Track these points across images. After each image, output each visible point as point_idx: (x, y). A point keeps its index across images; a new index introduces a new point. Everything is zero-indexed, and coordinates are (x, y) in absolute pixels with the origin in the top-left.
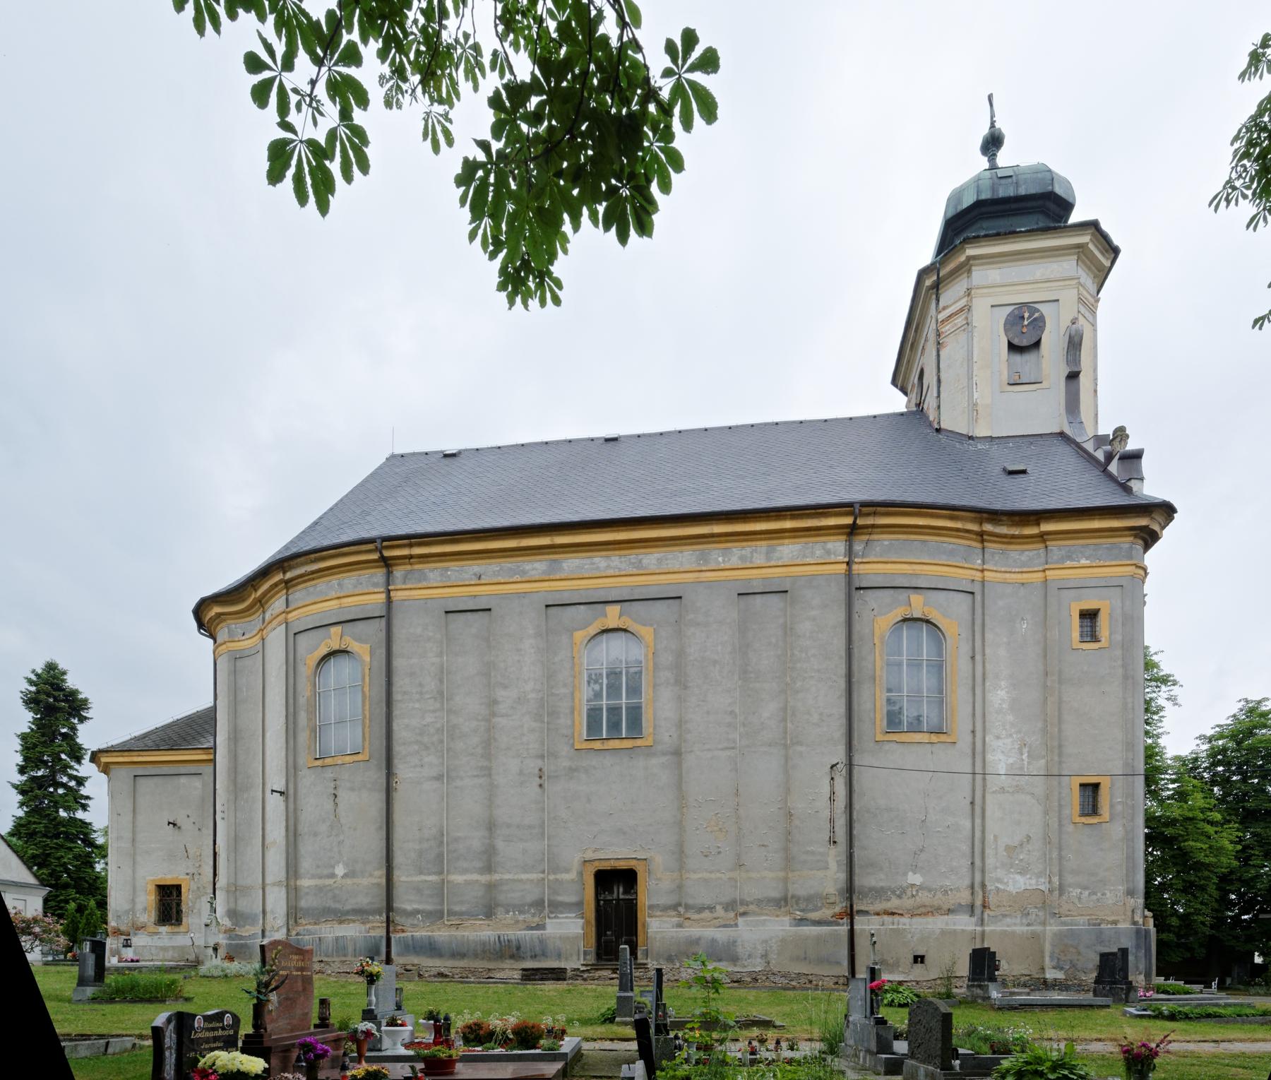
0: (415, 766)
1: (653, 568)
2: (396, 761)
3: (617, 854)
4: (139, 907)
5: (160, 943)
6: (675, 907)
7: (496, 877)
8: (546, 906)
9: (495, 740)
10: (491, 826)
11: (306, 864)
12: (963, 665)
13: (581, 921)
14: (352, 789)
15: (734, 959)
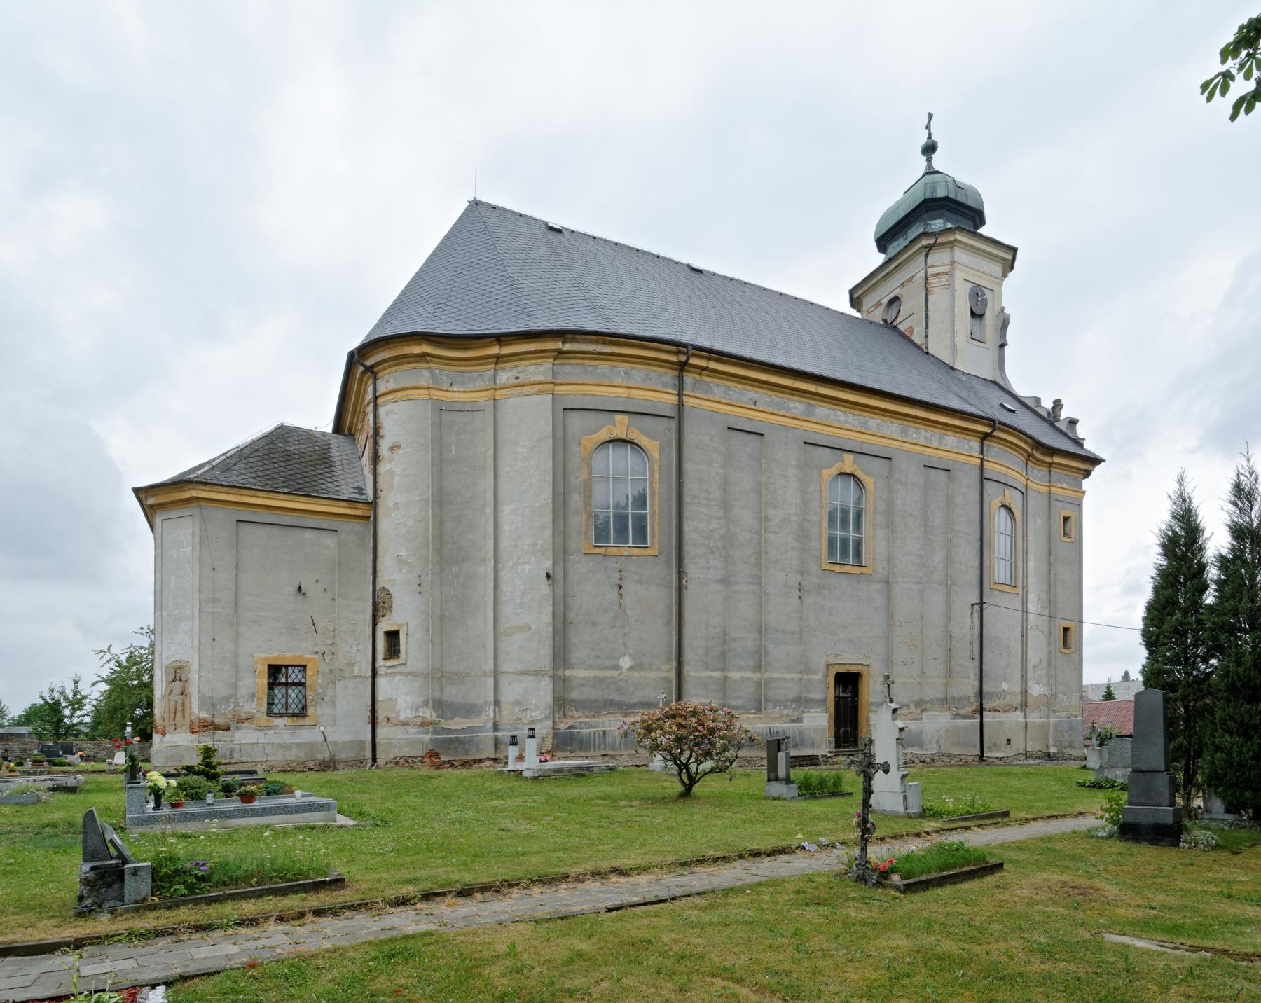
0: (703, 568)
1: (874, 431)
3: (849, 660)
4: (243, 692)
5: (276, 740)
7: (767, 675)
8: (802, 702)
9: (767, 553)
10: (761, 630)
11: (579, 653)
13: (827, 715)
14: (640, 582)
15: (921, 745)
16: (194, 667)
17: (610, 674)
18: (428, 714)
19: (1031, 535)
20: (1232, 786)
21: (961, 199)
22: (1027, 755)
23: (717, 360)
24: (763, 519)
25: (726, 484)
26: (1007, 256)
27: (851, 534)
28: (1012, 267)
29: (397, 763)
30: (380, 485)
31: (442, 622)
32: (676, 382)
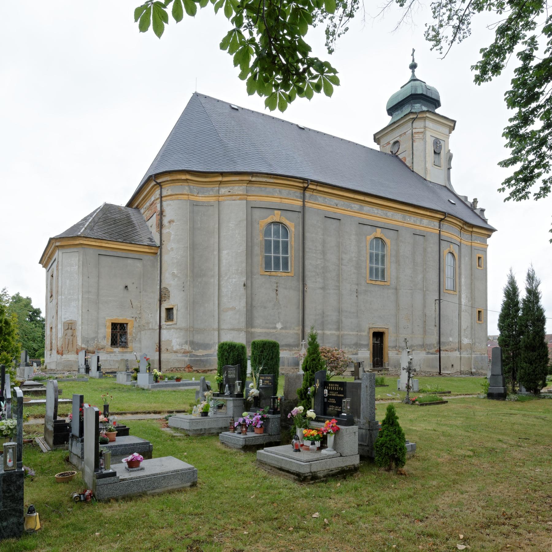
2: (306, 279)
3: (379, 326)
4: (101, 335)
6: (395, 347)
7: (342, 333)
8: (358, 345)
10: (340, 311)
11: (258, 321)
14: (286, 288)
16: (79, 323)
17: (272, 331)
18: (187, 348)
19: (463, 266)
20: (526, 381)
21: (429, 95)
22: (461, 373)
23: (320, 186)
24: (340, 259)
25: (324, 243)
26: (451, 125)
27: (380, 266)
28: (454, 129)
29: (172, 371)
30: (163, 239)
31: (194, 304)
32: (302, 196)
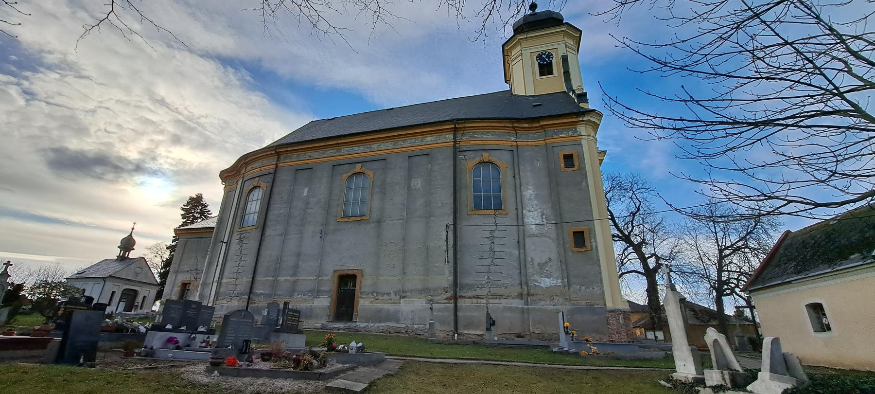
3: (350, 266)
8: (317, 293)
12: (510, 178)
